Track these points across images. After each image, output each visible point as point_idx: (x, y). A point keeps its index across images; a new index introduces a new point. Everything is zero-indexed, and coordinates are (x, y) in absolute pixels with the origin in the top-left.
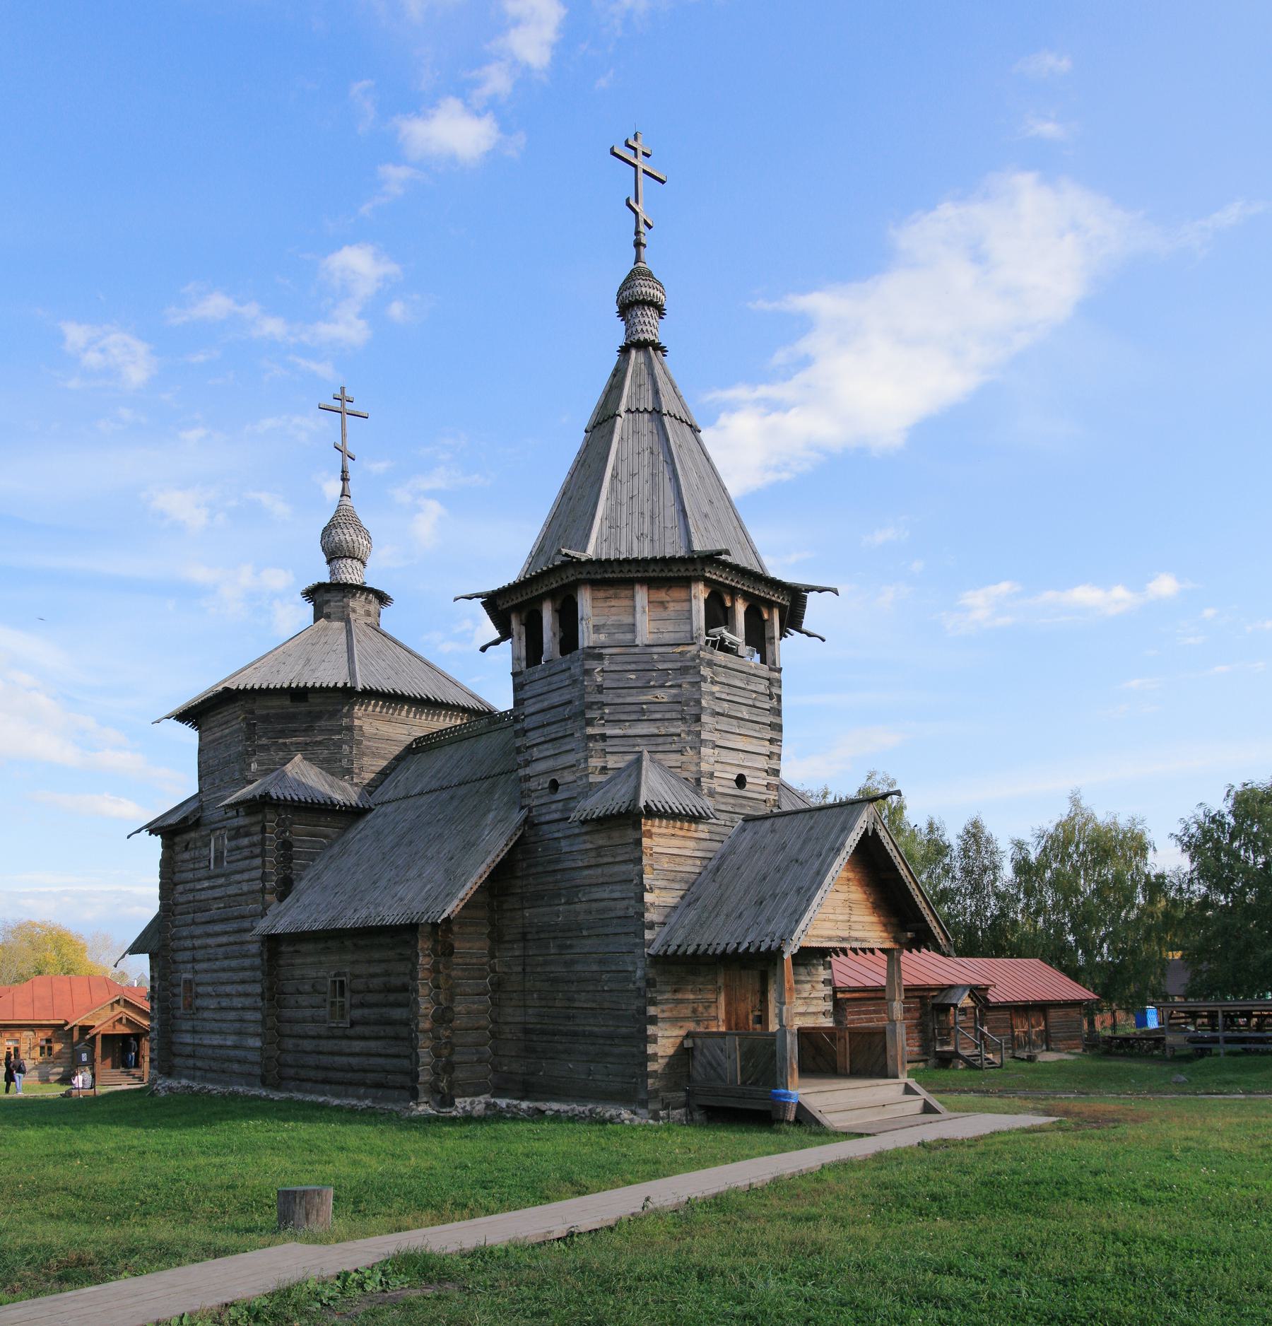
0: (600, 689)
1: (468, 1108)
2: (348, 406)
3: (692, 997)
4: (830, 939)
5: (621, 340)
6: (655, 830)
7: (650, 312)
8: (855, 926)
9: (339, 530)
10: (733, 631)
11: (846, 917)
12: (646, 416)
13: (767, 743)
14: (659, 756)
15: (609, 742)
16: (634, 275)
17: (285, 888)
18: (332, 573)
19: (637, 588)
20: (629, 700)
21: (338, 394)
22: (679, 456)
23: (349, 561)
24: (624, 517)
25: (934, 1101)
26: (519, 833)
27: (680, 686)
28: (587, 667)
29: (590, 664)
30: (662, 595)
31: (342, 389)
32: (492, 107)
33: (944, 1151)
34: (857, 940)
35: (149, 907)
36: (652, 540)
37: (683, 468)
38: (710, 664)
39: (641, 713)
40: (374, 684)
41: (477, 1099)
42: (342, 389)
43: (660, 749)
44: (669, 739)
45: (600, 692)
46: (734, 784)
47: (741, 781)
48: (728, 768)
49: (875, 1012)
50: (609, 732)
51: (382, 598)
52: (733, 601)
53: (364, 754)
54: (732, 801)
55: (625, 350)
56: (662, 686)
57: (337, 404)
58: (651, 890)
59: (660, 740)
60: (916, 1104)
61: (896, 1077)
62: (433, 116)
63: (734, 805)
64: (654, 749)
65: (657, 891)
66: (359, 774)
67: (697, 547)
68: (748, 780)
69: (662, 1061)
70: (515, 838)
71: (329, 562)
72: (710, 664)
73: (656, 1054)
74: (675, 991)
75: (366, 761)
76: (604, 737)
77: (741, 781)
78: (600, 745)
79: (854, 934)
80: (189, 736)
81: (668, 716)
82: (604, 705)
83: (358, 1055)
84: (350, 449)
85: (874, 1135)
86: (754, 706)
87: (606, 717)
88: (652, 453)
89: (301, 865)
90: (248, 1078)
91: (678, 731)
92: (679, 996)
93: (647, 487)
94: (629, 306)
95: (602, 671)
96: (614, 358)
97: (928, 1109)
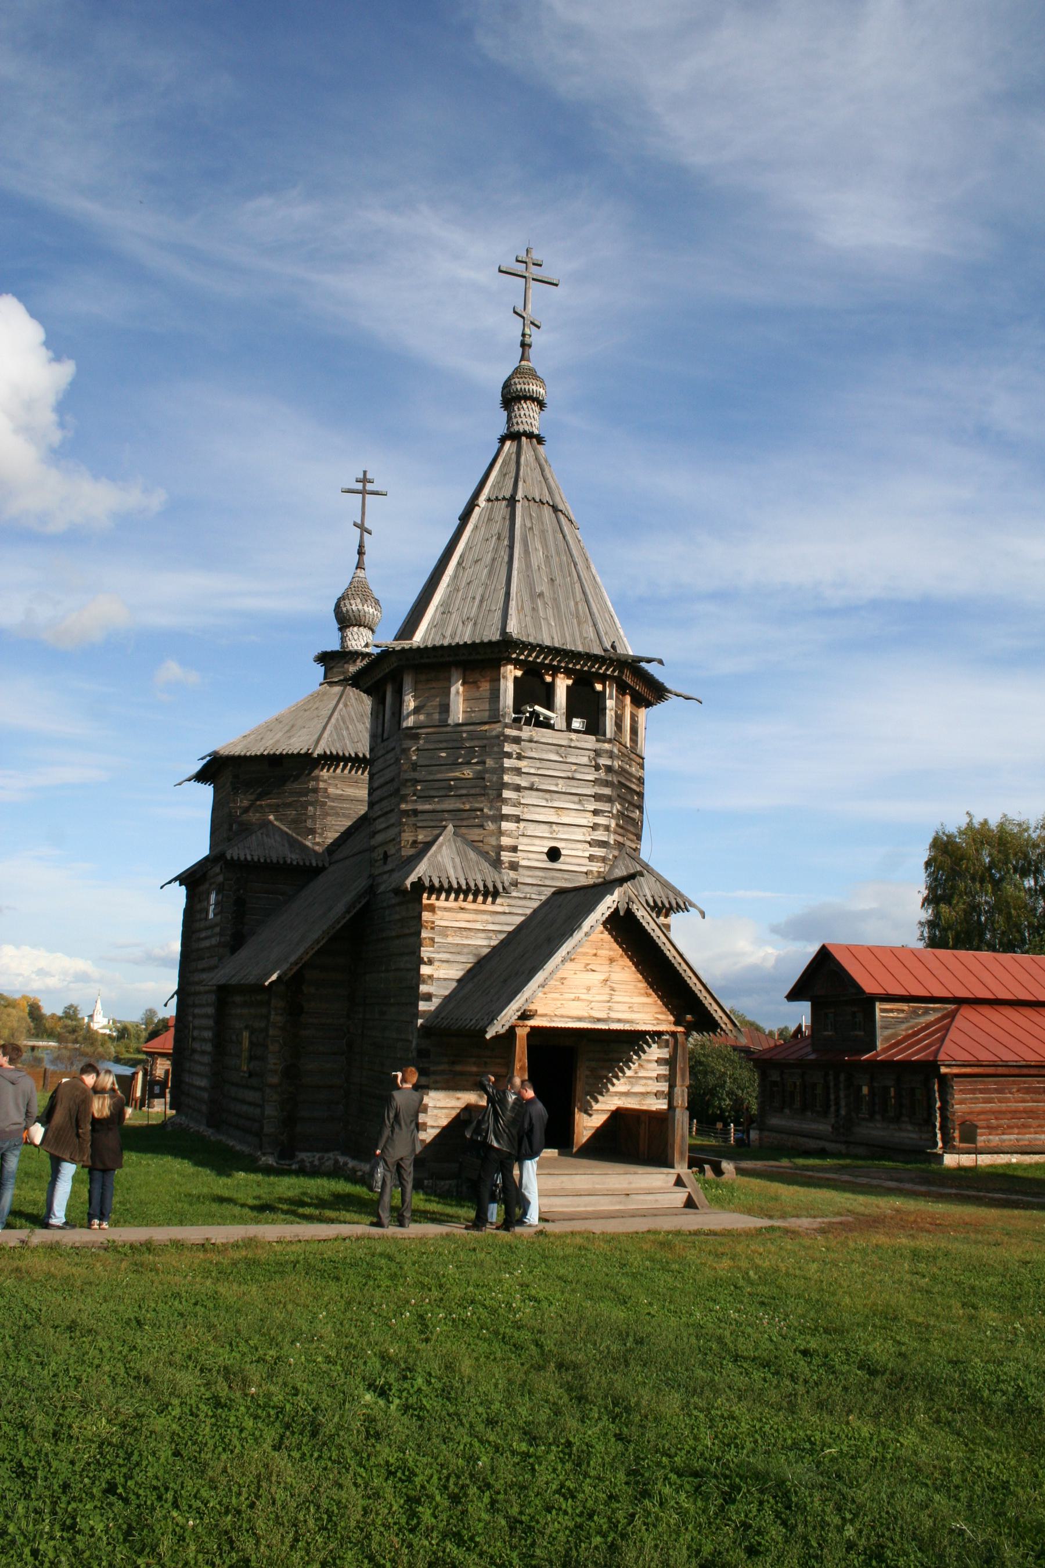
0: (415, 766)
1: (316, 1163)
2: (535, 271)
3: (474, 1069)
4: (580, 1019)
5: (502, 429)
6: (438, 904)
7: (535, 407)
8: (616, 1006)
9: (347, 602)
10: (550, 705)
11: (606, 998)
12: (504, 503)
13: (587, 846)
14: (464, 830)
15: (420, 817)
16: (518, 372)
18: (343, 639)
19: (453, 670)
20: (439, 776)
21: (523, 256)
22: (585, 1206)
23: (356, 629)
24: (458, 602)
25: (699, 1198)
26: (364, 901)
27: (484, 763)
28: (404, 746)
29: (407, 743)
31: (365, 472)
32: (761, 1139)
33: (714, 1237)
34: (619, 1021)
35: (175, 987)
36: (475, 624)
37: (872, 1223)
38: (517, 740)
39: (446, 790)
40: (336, 749)
41: (326, 1156)
42: (365, 472)
43: (465, 824)
44: (473, 814)
45: (414, 770)
46: (545, 857)
47: (554, 854)
48: (537, 841)
49: (997, 1091)
50: (420, 807)
51: (540, 440)
52: (554, 676)
53: (327, 814)
54: (540, 874)
55: (502, 440)
56: (469, 763)
57: (520, 268)
58: (430, 962)
59: (465, 815)
60: (680, 1197)
61: (672, 1167)
62: (24, 997)
63: (542, 878)
64: (459, 823)
65: (436, 964)
66: (321, 834)
67: (513, 628)
68: (563, 852)
69: (436, 1002)
70: (359, 906)
71: (340, 629)
72: (517, 740)
73: (430, 977)
74: (453, 1063)
75: (330, 820)
76: (416, 812)
77: (554, 854)
78: (413, 819)
79: (614, 1015)
80: (206, 792)
81: (473, 791)
82: (417, 781)
83: (250, 1104)
84: (530, 312)
85: (553, 1221)
86: (573, 778)
87: (418, 793)
88: (499, 538)
89: (728, 1132)
90: (911, 1181)
91: (481, 805)
92: (458, 1068)
93: (486, 571)
94: (511, 399)
95: (418, 749)
96: (497, 445)
97: (690, 1203)
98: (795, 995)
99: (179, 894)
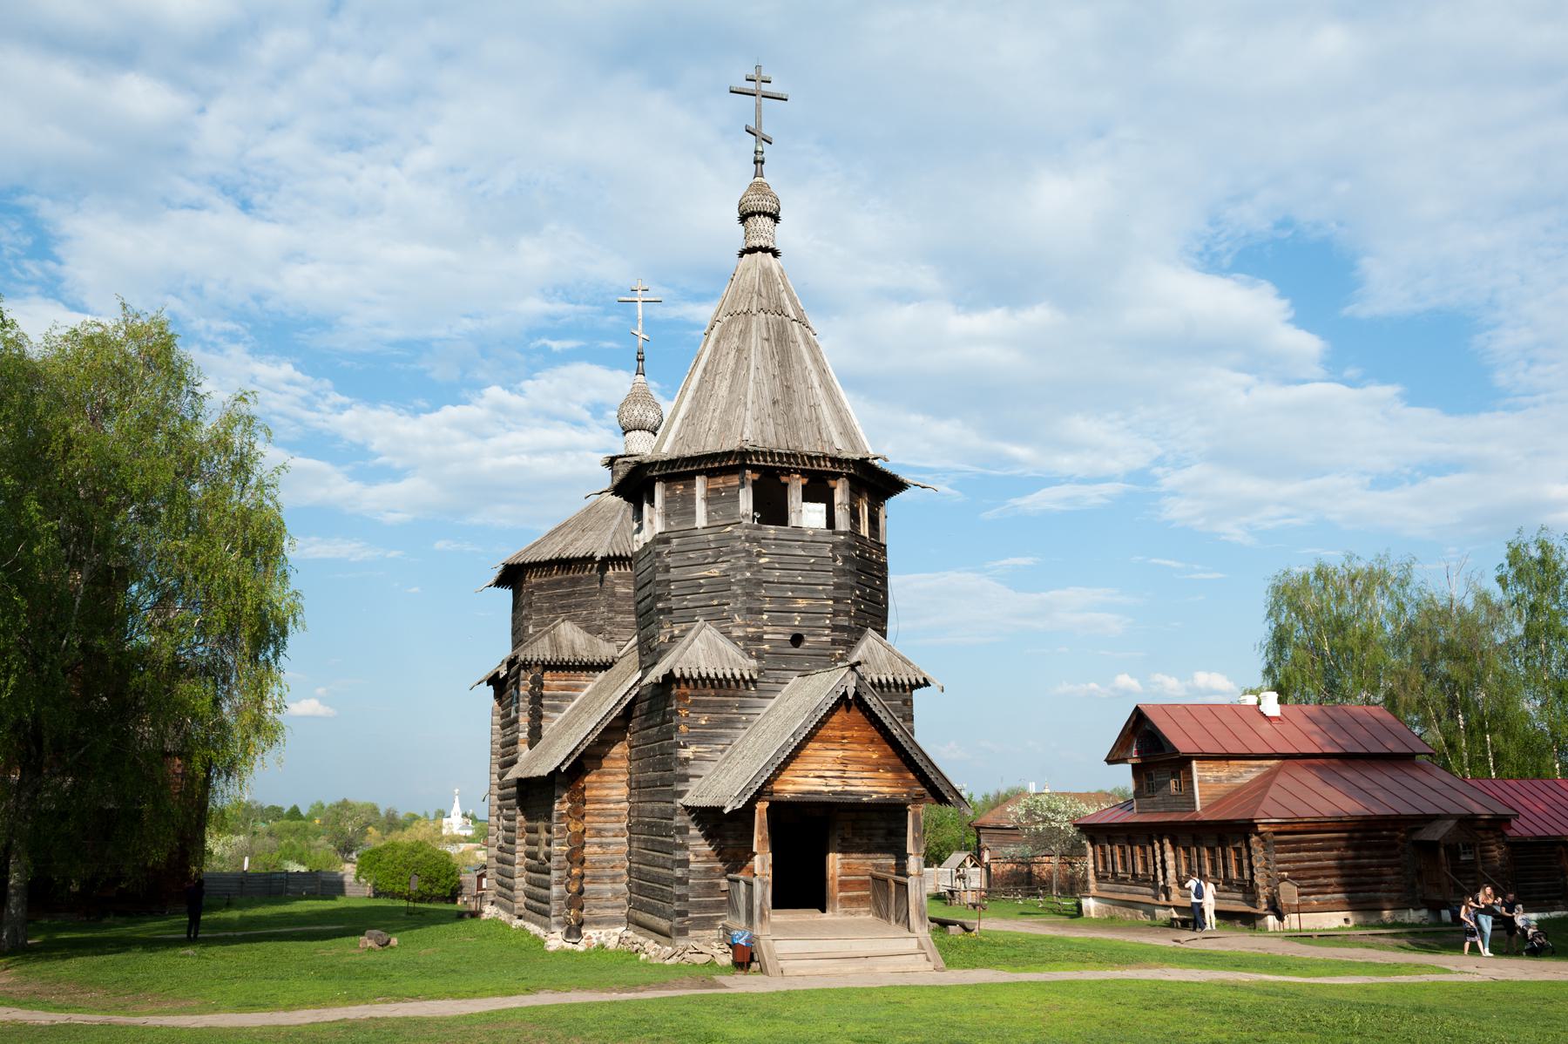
2: (765, 87)
17: (535, 735)
21: (752, 73)
30: (719, 482)
57: (751, 86)
80: (507, 594)
98: (1111, 760)
99: (507, 594)
